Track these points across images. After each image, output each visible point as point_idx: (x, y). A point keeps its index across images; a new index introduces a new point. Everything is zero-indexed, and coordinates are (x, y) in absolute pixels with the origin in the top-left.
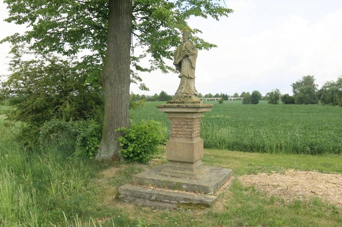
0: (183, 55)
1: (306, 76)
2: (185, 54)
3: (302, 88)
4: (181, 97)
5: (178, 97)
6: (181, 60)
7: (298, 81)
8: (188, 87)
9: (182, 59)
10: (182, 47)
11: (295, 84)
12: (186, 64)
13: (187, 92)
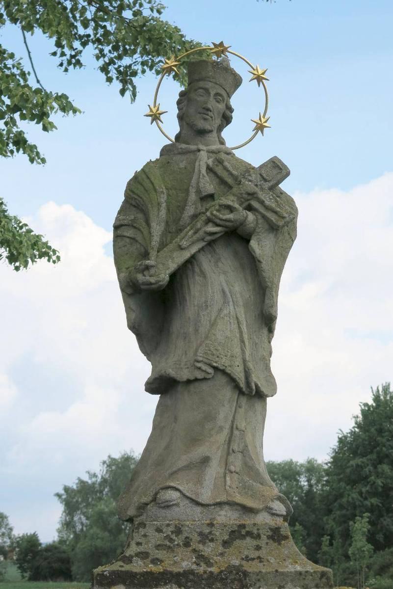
0: (209, 221)
1: (117, 456)
2: (231, 216)
3: (102, 506)
4: (205, 538)
5: (178, 531)
6: (187, 255)
7: (86, 478)
8: (237, 463)
9: (194, 250)
10: (190, 170)
11: (73, 490)
12: (219, 285)
13: (239, 499)
